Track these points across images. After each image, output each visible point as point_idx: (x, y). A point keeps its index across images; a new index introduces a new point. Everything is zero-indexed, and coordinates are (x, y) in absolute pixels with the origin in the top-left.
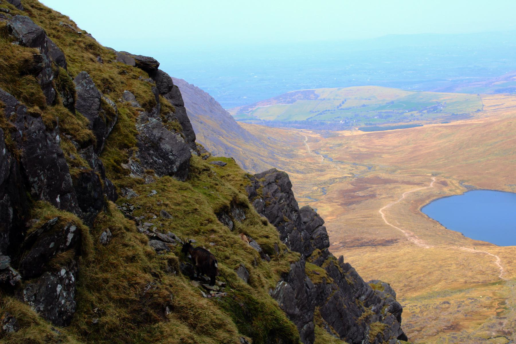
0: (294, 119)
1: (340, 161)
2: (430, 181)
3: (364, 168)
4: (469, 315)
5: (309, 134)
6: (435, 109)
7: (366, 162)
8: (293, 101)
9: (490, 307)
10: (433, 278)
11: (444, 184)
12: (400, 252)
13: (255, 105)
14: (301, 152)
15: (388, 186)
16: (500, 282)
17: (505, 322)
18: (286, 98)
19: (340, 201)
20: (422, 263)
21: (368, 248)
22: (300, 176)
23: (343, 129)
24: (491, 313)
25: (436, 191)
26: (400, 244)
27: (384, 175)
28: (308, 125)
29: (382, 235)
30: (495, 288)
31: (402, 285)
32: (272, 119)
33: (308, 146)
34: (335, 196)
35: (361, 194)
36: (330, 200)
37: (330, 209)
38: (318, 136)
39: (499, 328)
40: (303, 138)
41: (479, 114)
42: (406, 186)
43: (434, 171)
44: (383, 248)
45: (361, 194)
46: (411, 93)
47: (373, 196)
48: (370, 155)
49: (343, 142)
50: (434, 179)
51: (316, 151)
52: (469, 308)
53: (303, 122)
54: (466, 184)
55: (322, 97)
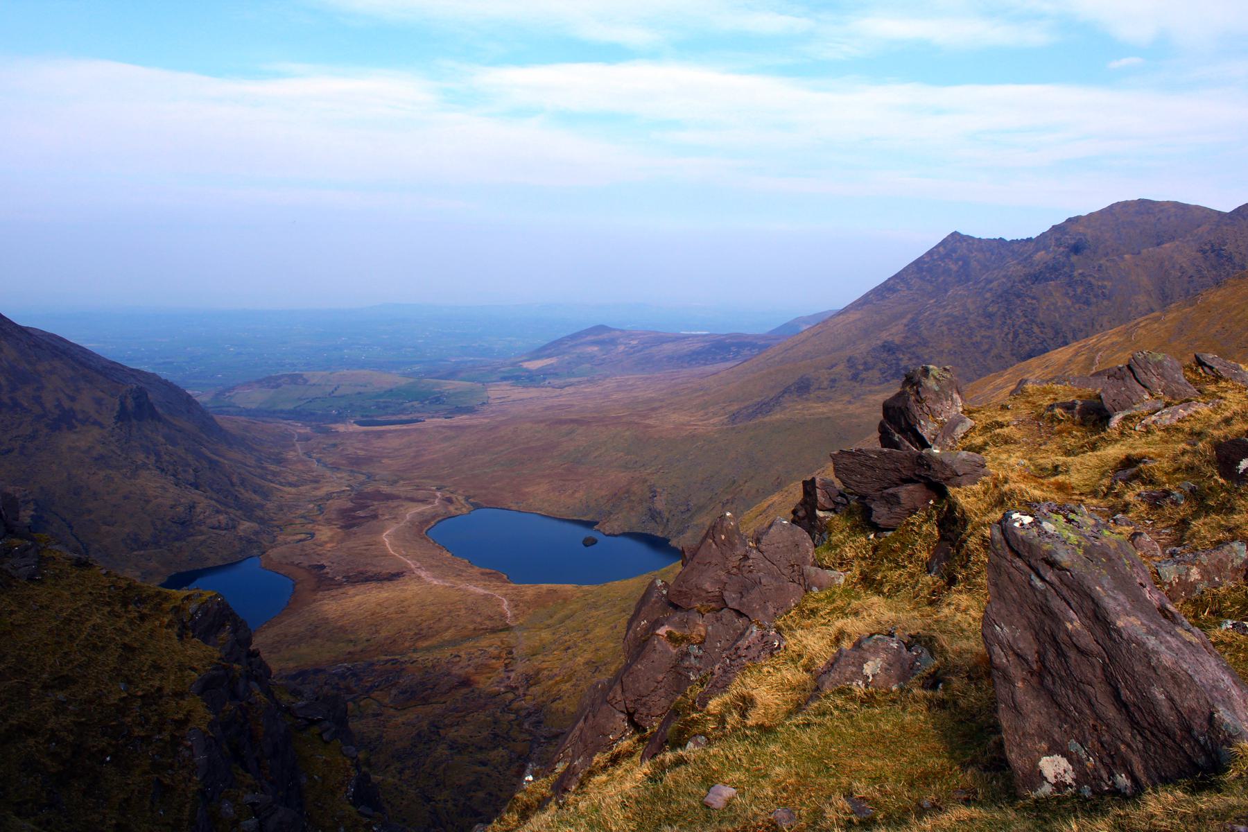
0: (280, 407)
1: (336, 468)
3: (362, 478)
4: (480, 668)
5: (301, 429)
6: (437, 400)
7: (365, 469)
8: (278, 386)
9: (498, 658)
11: (450, 501)
12: (406, 591)
13: (233, 388)
14: (291, 455)
15: (390, 503)
16: (508, 628)
17: (513, 675)
18: (271, 382)
19: (340, 523)
20: (432, 608)
21: (373, 584)
22: (293, 490)
23: (336, 422)
24: (499, 664)
25: (442, 510)
26: (407, 579)
27: (385, 489)
28: (297, 415)
29: (387, 568)
30: (503, 635)
32: (253, 406)
33: (298, 446)
34: (333, 516)
35: (361, 513)
36: (329, 522)
37: (330, 534)
38: (308, 430)
39: (507, 682)
40: (292, 436)
41: (485, 407)
42: (411, 504)
43: (438, 483)
44: (389, 583)
45: (361, 513)
46: (411, 380)
47: (375, 517)
48: (369, 460)
49: (337, 441)
50: (438, 494)
51: (308, 454)
52: (479, 661)
53: (289, 412)
54: (471, 500)
55: (313, 382)
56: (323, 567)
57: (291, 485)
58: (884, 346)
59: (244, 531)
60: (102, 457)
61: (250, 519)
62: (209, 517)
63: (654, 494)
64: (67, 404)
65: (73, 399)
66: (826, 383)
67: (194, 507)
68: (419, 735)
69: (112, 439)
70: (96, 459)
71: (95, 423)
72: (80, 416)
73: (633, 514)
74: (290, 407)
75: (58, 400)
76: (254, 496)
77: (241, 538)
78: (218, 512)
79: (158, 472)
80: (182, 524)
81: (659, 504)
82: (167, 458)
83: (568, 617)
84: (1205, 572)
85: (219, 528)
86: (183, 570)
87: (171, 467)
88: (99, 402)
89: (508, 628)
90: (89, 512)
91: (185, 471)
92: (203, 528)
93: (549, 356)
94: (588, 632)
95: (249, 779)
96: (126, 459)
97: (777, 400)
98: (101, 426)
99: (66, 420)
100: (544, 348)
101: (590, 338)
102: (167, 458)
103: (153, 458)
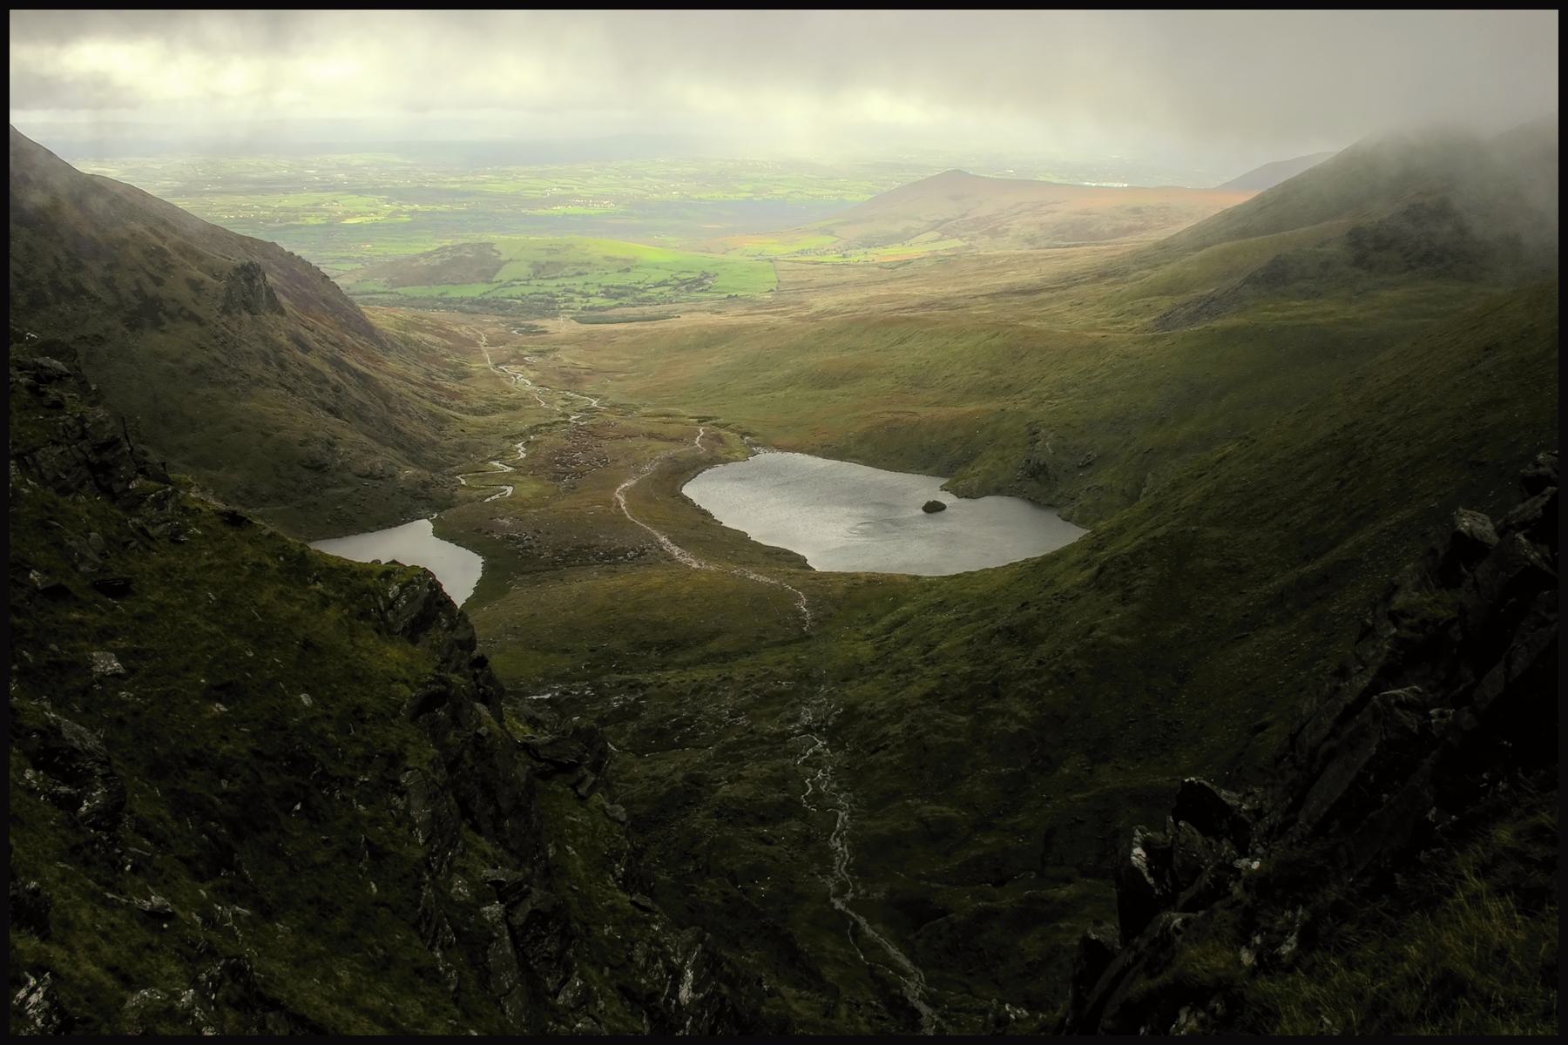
14: (475, 366)
57: (475, 412)
59: (407, 480)
61: (415, 462)
64: (151, 289)
65: (159, 282)
70: (193, 372)
75: (137, 282)
79: (283, 391)
83: (898, 624)
84: (1402, 958)
92: (348, 476)
94: (931, 647)
95: (485, 844)
98: (199, 321)
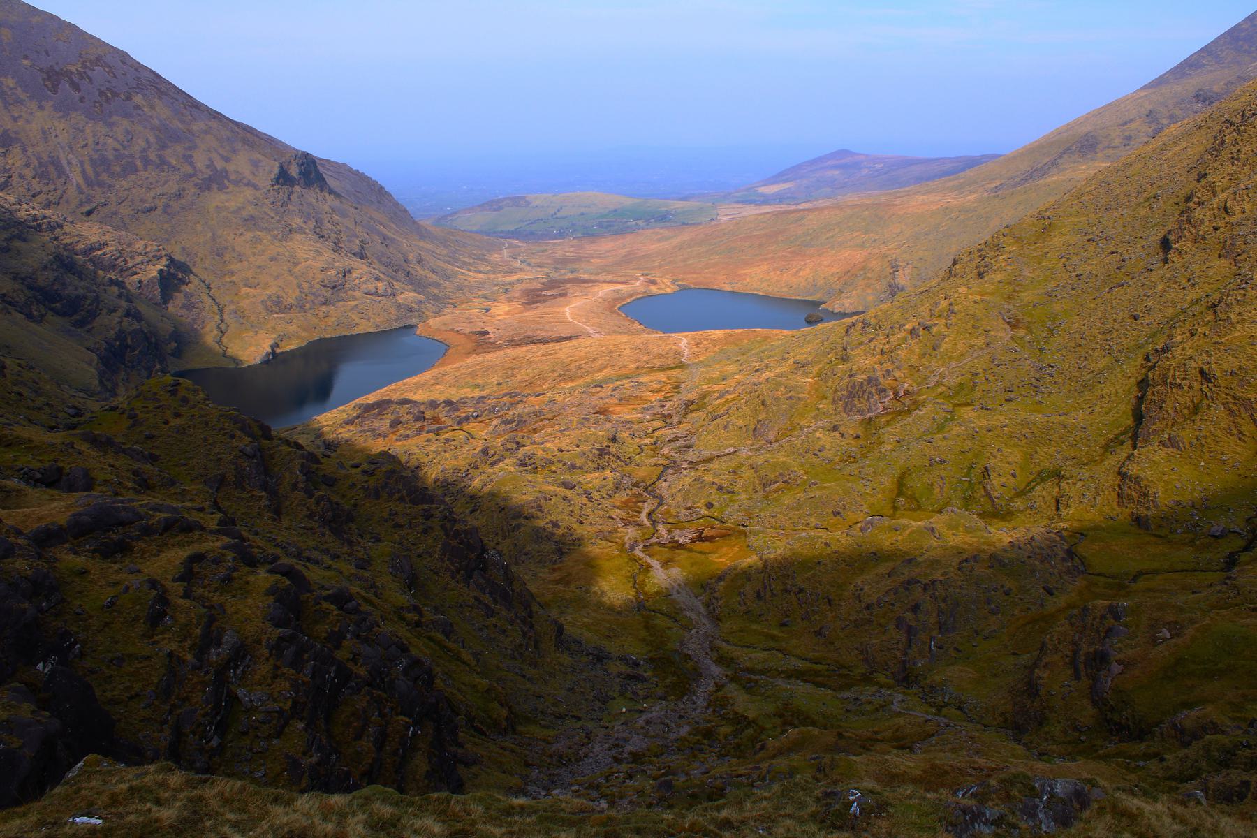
2: (637, 279)
7: (569, 266)
8: (499, 209)
10: (598, 364)
13: (456, 213)
16: (681, 366)
18: (494, 205)
31: (556, 374)
35: (549, 293)
37: (507, 309)
45: (549, 293)
46: (637, 201)
47: (564, 295)
53: (512, 232)
56: (487, 333)
58: (1197, 96)
59: (405, 299)
60: (252, 218)
62: (365, 283)
63: (895, 268)
64: (219, 164)
65: (227, 160)
66: (1117, 142)
67: (350, 272)
68: (485, 451)
69: (267, 202)
70: (246, 220)
71: (249, 184)
72: (233, 177)
73: (869, 291)
74: (512, 229)
76: (430, 275)
77: (399, 306)
78: (378, 279)
79: (316, 237)
80: (334, 287)
81: (902, 279)
82: (331, 226)
85: (376, 293)
86: (328, 336)
87: (333, 235)
88: (256, 164)
89: (681, 366)
90: (232, 273)
91: (350, 241)
93: (786, 181)
96: (279, 221)
97: (1053, 164)
98: (256, 187)
99: (216, 180)
100: (781, 174)
101: (834, 162)
102: (331, 226)
103: (312, 224)
